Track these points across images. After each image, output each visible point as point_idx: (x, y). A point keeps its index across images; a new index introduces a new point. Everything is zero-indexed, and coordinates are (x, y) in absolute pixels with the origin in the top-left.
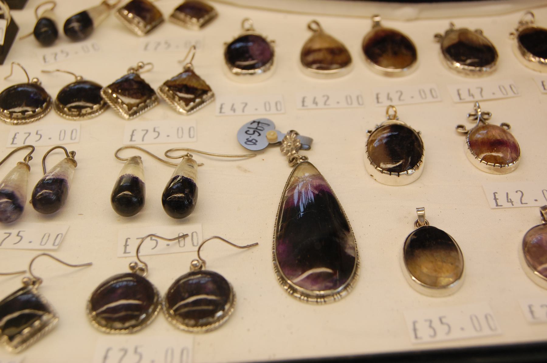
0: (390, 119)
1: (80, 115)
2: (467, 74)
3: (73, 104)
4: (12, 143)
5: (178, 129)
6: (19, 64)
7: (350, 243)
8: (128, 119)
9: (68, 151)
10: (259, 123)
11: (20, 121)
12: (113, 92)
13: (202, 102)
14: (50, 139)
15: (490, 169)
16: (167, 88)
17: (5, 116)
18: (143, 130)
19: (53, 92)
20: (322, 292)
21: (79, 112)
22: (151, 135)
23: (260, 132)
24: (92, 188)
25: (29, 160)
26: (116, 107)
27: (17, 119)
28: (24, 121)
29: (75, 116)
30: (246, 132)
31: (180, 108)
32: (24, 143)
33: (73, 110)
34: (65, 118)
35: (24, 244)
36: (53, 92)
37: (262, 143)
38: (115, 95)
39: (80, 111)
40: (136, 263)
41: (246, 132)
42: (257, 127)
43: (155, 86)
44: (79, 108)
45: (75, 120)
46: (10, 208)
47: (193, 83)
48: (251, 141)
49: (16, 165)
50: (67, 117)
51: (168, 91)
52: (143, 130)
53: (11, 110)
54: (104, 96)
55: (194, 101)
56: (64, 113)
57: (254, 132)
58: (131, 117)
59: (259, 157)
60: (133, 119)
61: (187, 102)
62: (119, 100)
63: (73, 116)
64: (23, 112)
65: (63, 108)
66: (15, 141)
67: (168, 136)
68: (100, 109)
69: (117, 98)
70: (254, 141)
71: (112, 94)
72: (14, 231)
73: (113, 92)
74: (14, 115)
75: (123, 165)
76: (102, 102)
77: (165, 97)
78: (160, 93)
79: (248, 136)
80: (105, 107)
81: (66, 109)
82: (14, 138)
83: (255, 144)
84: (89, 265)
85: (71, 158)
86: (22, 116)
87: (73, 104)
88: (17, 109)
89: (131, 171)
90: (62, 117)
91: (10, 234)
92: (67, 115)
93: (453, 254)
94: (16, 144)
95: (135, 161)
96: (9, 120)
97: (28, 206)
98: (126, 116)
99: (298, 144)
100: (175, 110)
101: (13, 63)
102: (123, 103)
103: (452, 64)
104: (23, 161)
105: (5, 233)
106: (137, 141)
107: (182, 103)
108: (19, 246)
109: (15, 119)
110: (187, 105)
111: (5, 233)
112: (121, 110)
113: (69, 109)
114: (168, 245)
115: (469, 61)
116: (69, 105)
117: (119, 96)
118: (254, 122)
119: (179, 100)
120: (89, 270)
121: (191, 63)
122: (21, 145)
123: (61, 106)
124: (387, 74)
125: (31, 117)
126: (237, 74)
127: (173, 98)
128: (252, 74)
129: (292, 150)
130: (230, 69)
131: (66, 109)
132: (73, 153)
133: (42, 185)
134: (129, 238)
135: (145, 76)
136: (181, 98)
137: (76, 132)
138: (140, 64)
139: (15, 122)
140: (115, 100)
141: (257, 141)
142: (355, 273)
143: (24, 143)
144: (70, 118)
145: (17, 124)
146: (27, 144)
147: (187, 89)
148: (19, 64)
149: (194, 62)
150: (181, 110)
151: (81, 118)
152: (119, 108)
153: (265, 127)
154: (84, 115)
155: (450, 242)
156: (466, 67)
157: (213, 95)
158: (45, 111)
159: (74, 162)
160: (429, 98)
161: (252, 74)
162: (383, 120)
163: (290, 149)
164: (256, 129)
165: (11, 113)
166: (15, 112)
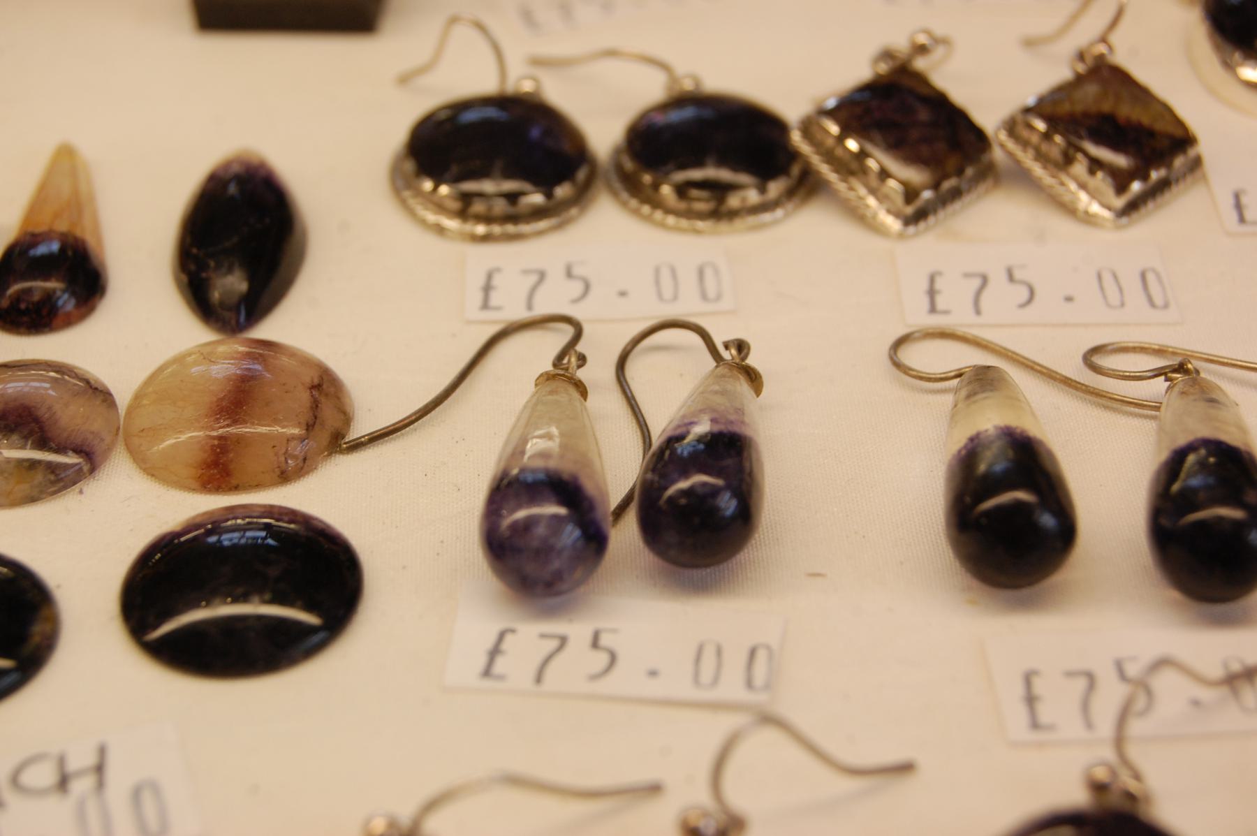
1: (719, 214)
3: (696, 174)
4: (485, 305)
5: (1100, 277)
6: (480, 27)
8: (901, 236)
9: (719, 342)
11: (497, 229)
12: (846, 131)
13: (1164, 185)
14: (623, 294)
16: (1041, 125)
17: (440, 208)
18: (967, 275)
19: (603, 134)
21: (717, 205)
22: (1002, 298)
24: (857, 474)
25: (579, 367)
26: (851, 189)
27: (488, 219)
28: (510, 228)
29: (702, 216)
31: (1094, 199)
32: (530, 306)
33: (695, 193)
34: (662, 225)
35: (623, 681)
36: (603, 134)
38: (852, 145)
39: (721, 200)
40: (1113, 773)
43: (988, 116)
44: (719, 190)
45: (697, 232)
46: (571, 534)
47: (1127, 111)
49: (531, 388)
50: (671, 220)
51: (1047, 136)
52: (967, 275)
53: (470, 186)
54: (805, 148)
55: (1145, 178)
56: (657, 204)
58: (911, 229)
60: (916, 235)
61: (1121, 181)
62: (872, 164)
63: (690, 214)
64: (512, 198)
65: (656, 186)
66: (495, 299)
67: (1069, 299)
68: (790, 193)
69: (862, 155)
71: (841, 139)
72: (577, 630)
73: (846, 131)
74: (478, 207)
75: (949, 399)
76: (796, 170)
77: (1027, 159)
78: (1011, 145)
80: (806, 186)
81: (666, 190)
82: (487, 288)
84: (905, 768)
85: (737, 363)
86: (510, 210)
87: (696, 174)
88: (488, 186)
89: (989, 419)
90: (648, 219)
91: (563, 640)
92: (668, 211)
94: (498, 308)
95: (982, 381)
96: (452, 224)
97: (626, 536)
98: (893, 224)
100: (1069, 210)
101: (454, 20)
102: (884, 174)
104: (549, 367)
105: (543, 636)
106: (959, 316)
107: (1100, 181)
108: (610, 685)
109: (480, 219)
110: (1121, 188)
111: (543, 636)
112: (872, 201)
113: (682, 190)
114: (1196, 703)
116: (681, 176)
117: (870, 148)
119: (1092, 172)
120: (904, 788)
121: (1103, 40)
122: (519, 313)
123: (647, 178)
125: (538, 213)
127: (1068, 160)
130: (1229, 67)
131: (666, 190)
132: (741, 347)
133: (666, 459)
135: (953, 78)
136: (1095, 165)
137: (717, 272)
138: (922, 39)
139: (481, 229)
140: (854, 165)
143: (530, 306)
144: (684, 223)
145: (486, 238)
146: (543, 307)
147: (1109, 130)
148: (480, 27)
149: (1114, 38)
150: (1095, 208)
151: (723, 226)
152: (862, 191)
154: (733, 215)
157: (1197, 163)
158: (581, 197)
159: (753, 377)
165: (467, 199)
166: (481, 195)
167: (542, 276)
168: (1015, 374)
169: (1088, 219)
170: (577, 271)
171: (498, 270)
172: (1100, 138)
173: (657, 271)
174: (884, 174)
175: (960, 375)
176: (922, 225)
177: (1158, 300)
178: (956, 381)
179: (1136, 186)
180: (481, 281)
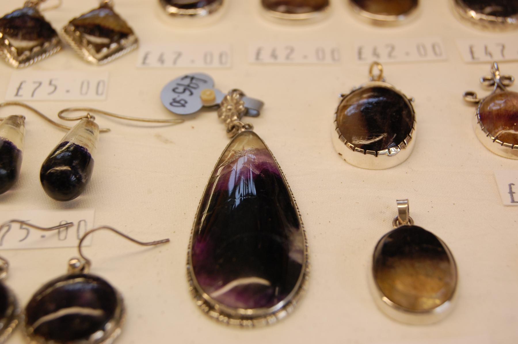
0: (373, 80)
2: (484, 27)
4: (17, 95)
7: (297, 244)
8: (18, 68)
10: (192, 78)
15: (506, 152)
20: (250, 312)
23: (193, 90)
30: (174, 90)
37: (194, 104)
41: (174, 90)
42: (190, 83)
48: (178, 102)
57: (184, 90)
58: (22, 65)
59: (188, 124)
60: (24, 67)
61: (98, 48)
70: (183, 102)
79: (175, 96)
83: (183, 106)
93: (443, 265)
98: (14, 63)
99: (241, 107)
103: (466, 12)
114: (43, 237)
115: (488, 10)
118: (186, 77)
124: (376, 23)
126: (173, 15)
128: (191, 15)
129: (233, 115)
134: (513, 184)
141: (186, 102)
142: (300, 287)
153: (201, 84)
155: (440, 249)
156: (484, 17)
157: (136, 41)
160: (431, 55)
161: (191, 15)
162: (364, 81)
163: (230, 114)
164: (189, 86)
167: (40, 84)
168: (29, 116)
169: (89, 63)
170: (54, 82)
171: (25, 82)
172: (91, 32)
173: (82, 84)
174: (10, 45)
175: (81, 119)
176: (27, 64)
177: (100, 91)
178: (78, 121)
179: (105, 51)
180: (17, 85)
